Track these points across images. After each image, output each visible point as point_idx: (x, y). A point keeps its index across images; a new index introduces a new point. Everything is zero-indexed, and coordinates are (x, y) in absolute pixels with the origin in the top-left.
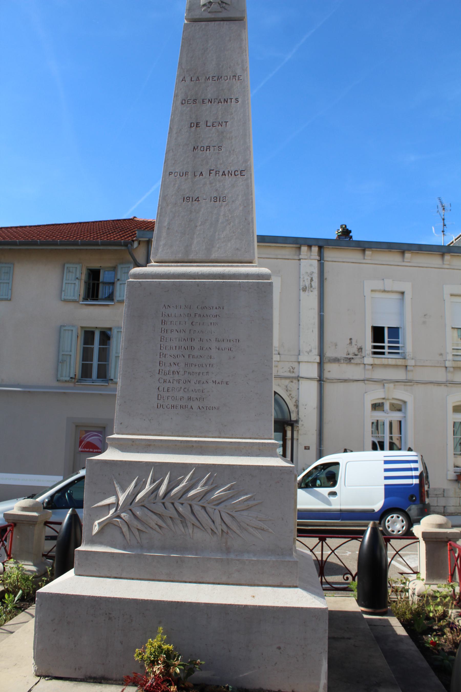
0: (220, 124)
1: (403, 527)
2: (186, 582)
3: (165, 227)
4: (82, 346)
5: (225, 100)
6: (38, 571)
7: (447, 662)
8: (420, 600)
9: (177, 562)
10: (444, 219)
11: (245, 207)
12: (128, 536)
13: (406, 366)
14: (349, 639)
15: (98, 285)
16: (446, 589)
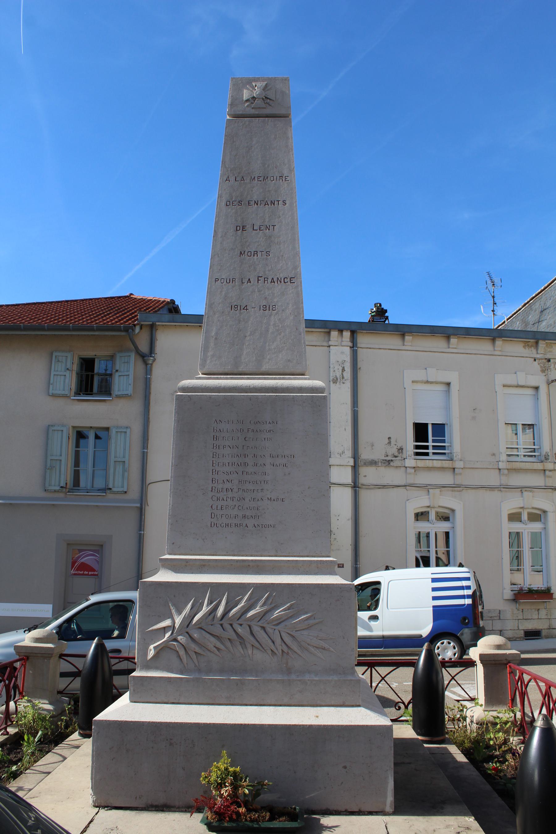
0: (267, 228)
1: (455, 654)
2: (246, 705)
5: (271, 201)
6: (55, 709)
7: (511, 785)
8: (479, 728)
10: (493, 297)
11: (296, 316)
12: (185, 660)
13: (454, 469)
14: (410, 763)
15: (92, 377)
16: (507, 714)
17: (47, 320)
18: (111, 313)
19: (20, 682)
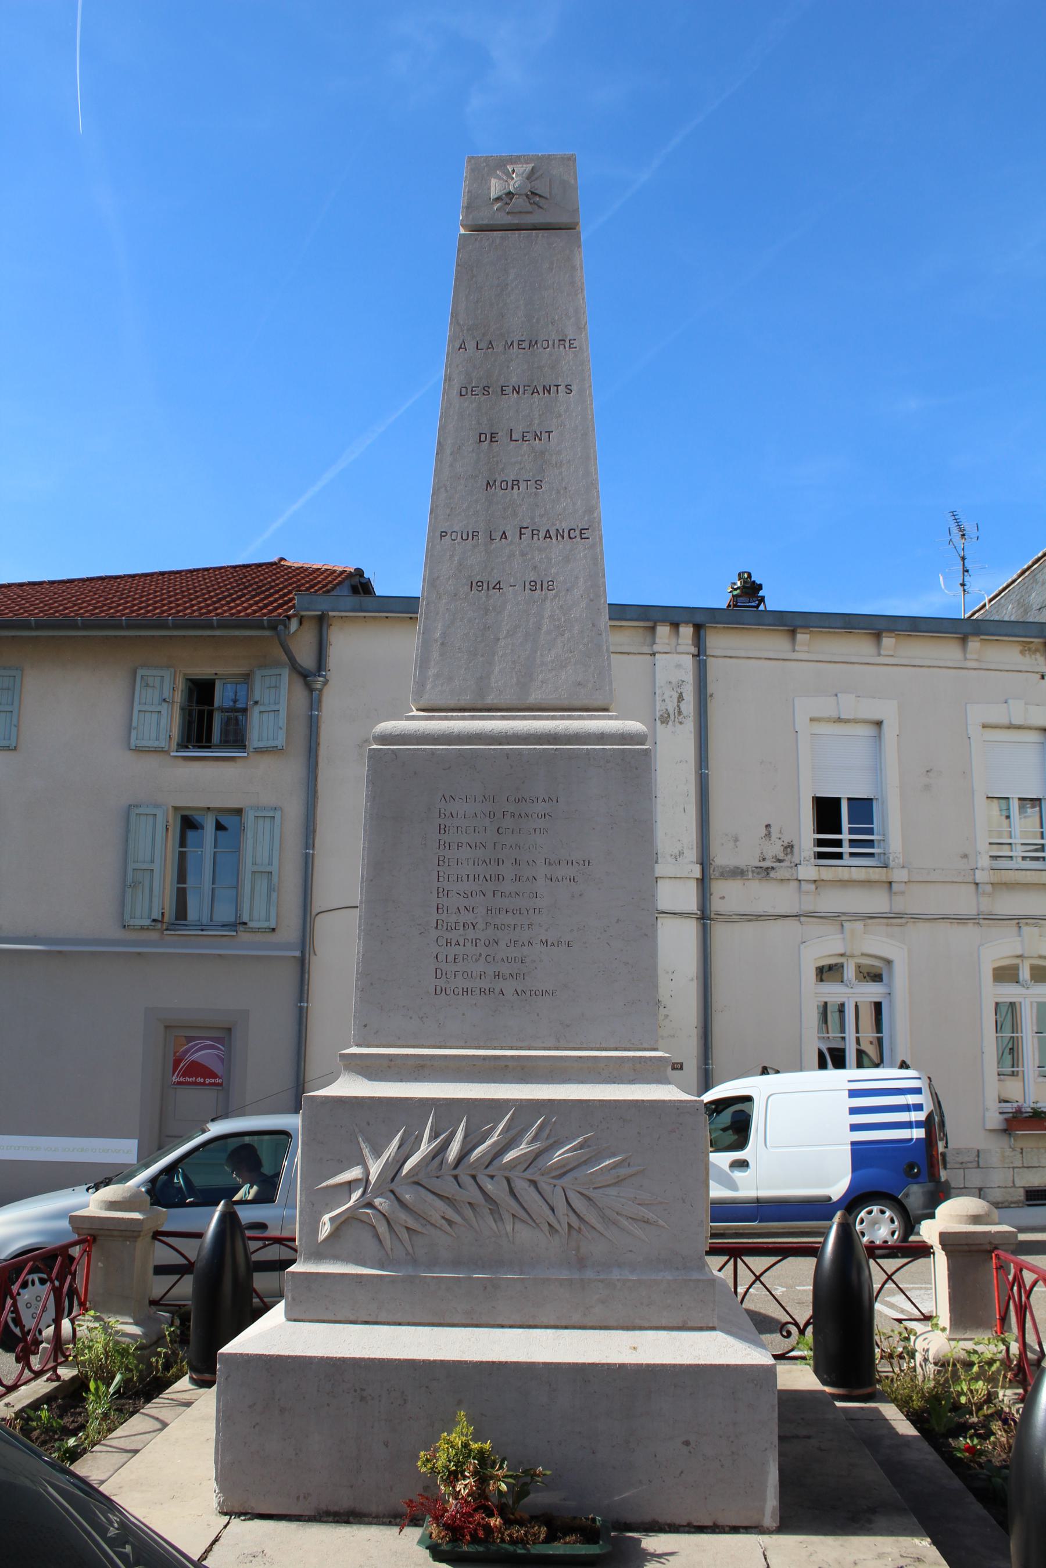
0: (537, 436)
1: (893, 1233)
2: (502, 1327)
3: (437, 641)
5: (544, 387)
7: (999, 1480)
8: (939, 1372)
10: (963, 559)
11: (591, 600)
14: (809, 1437)
15: (211, 714)
16: (992, 1347)
17: (126, 608)
18: (244, 595)
19: (80, 1285)
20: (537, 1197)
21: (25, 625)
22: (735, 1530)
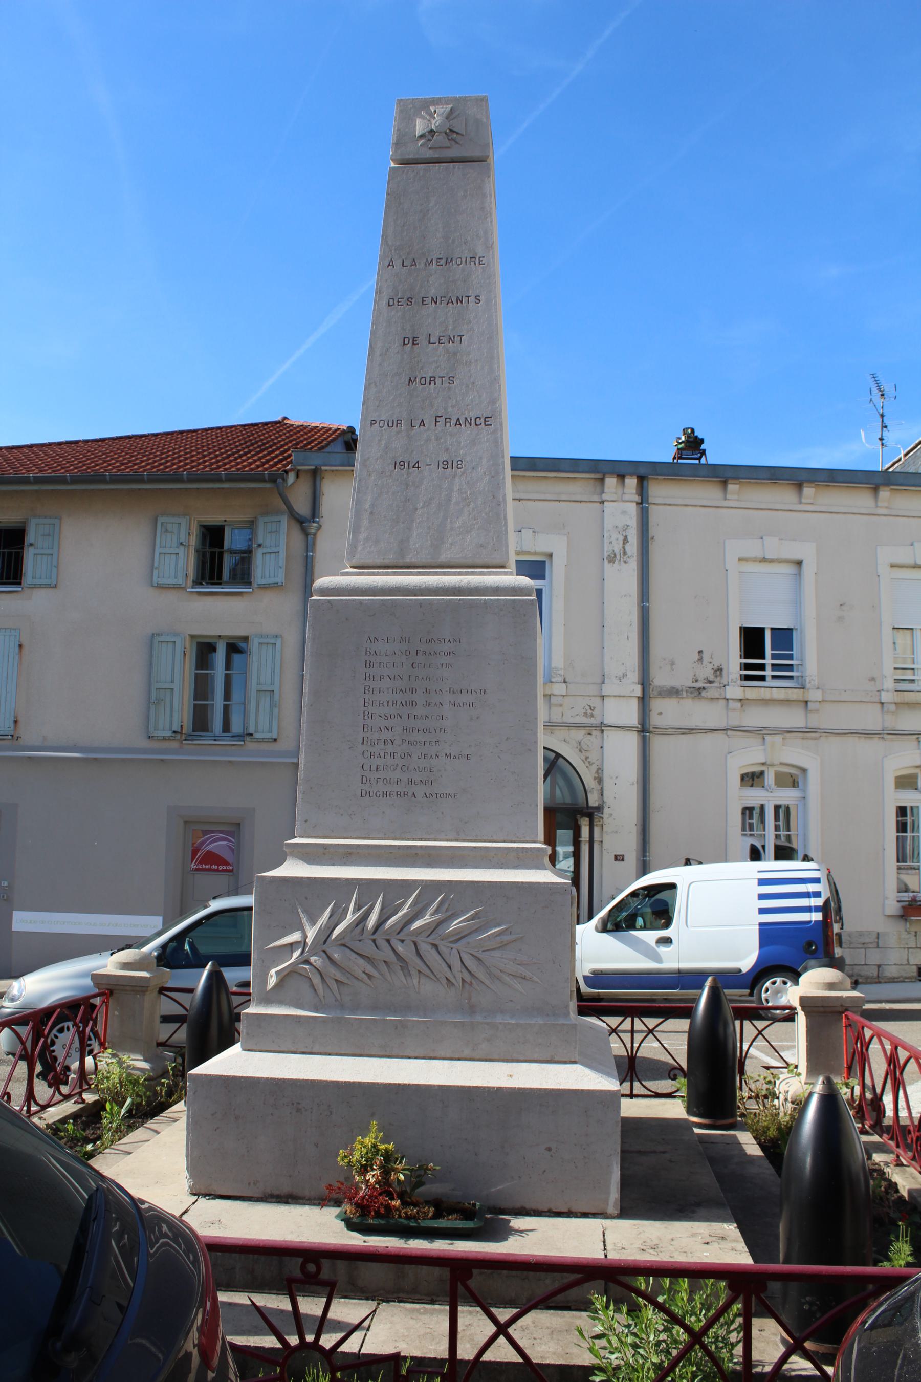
0: (451, 340)
2: (409, 1058)
4: (194, 671)
6: (153, 1069)
8: (795, 1109)
9: (396, 1028)
10: (882, 416)
12: (321, 991)
13: (806, 702)
14: (664, 1152)
17: (148, 464)
18: (249, 452)
19: (100, 1028)
20: (438, 957)
21: (62, 480)
22: (585, 1215)
